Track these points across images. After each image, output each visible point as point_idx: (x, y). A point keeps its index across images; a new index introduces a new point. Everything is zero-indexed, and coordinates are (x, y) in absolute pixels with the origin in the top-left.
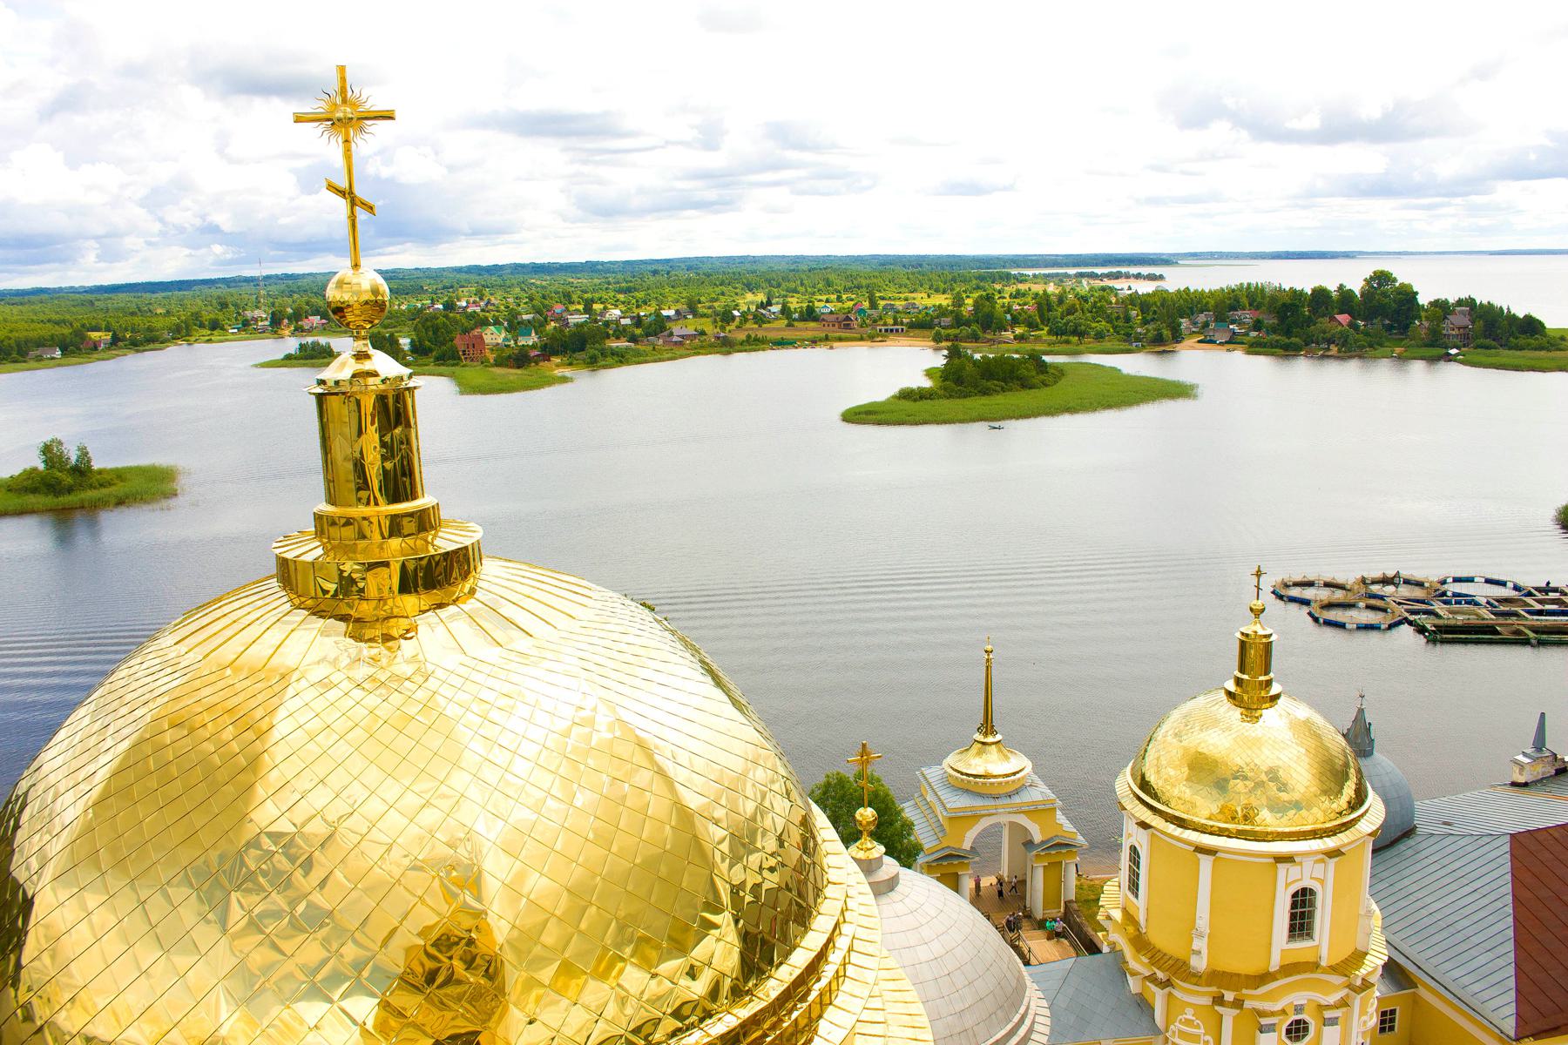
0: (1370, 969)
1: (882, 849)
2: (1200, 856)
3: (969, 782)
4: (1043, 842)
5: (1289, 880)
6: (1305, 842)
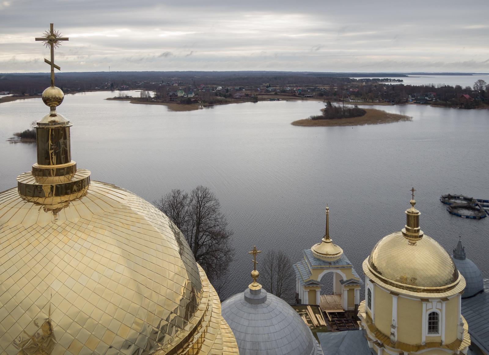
0: (463, 348)
1: (261, 286)
2: (392, 295)
3: (320, 256)
4: (347, 281)
5: (427, 309)
6: (433, 293)
